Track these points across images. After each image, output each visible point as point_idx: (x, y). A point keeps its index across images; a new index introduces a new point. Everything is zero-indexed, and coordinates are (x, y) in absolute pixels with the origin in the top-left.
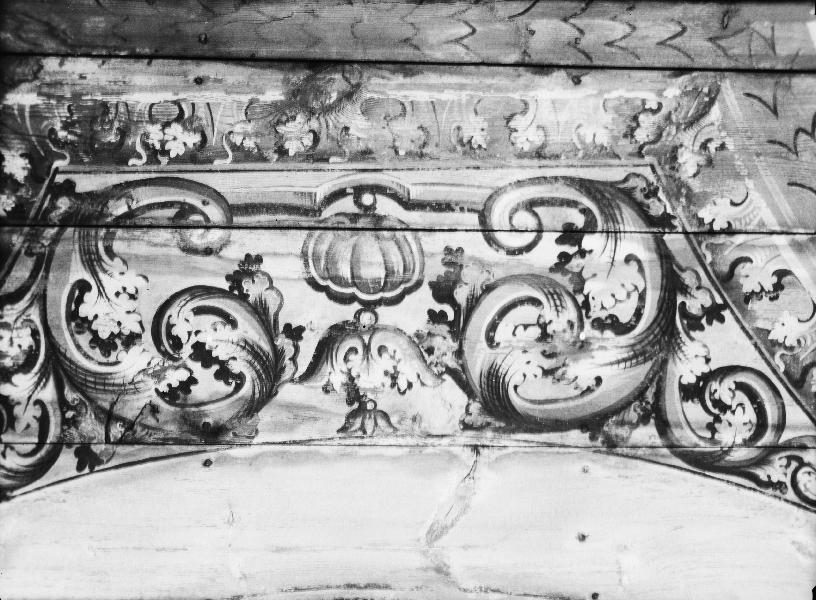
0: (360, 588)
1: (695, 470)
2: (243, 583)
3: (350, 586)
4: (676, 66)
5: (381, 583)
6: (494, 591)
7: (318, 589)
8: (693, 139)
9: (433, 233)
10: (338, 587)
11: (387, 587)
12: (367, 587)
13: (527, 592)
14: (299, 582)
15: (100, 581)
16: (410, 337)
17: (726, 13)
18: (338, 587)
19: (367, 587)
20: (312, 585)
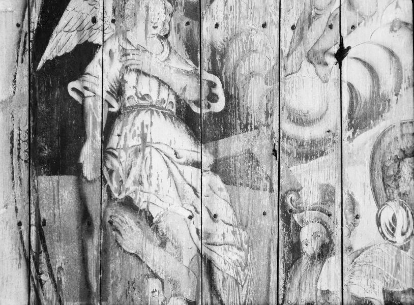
0: (13, 147)
1: (104, 125)
2: (10, 207)
3: (12, 152)
4: (23, 10)
5: (10, 136)
6: (15, 78)
7: (13, 168)
8: (154, 205)
9: (368, 61)
10: (12, 158)
11: (12, 132)
12: (12, 143)
13: (16, 60)
14: (9, 178)
15: (7, 281)
16: (400, 193)
17: (407, 24)
18: (12, 158)
19: (12, 143)
20: (10, 172)
